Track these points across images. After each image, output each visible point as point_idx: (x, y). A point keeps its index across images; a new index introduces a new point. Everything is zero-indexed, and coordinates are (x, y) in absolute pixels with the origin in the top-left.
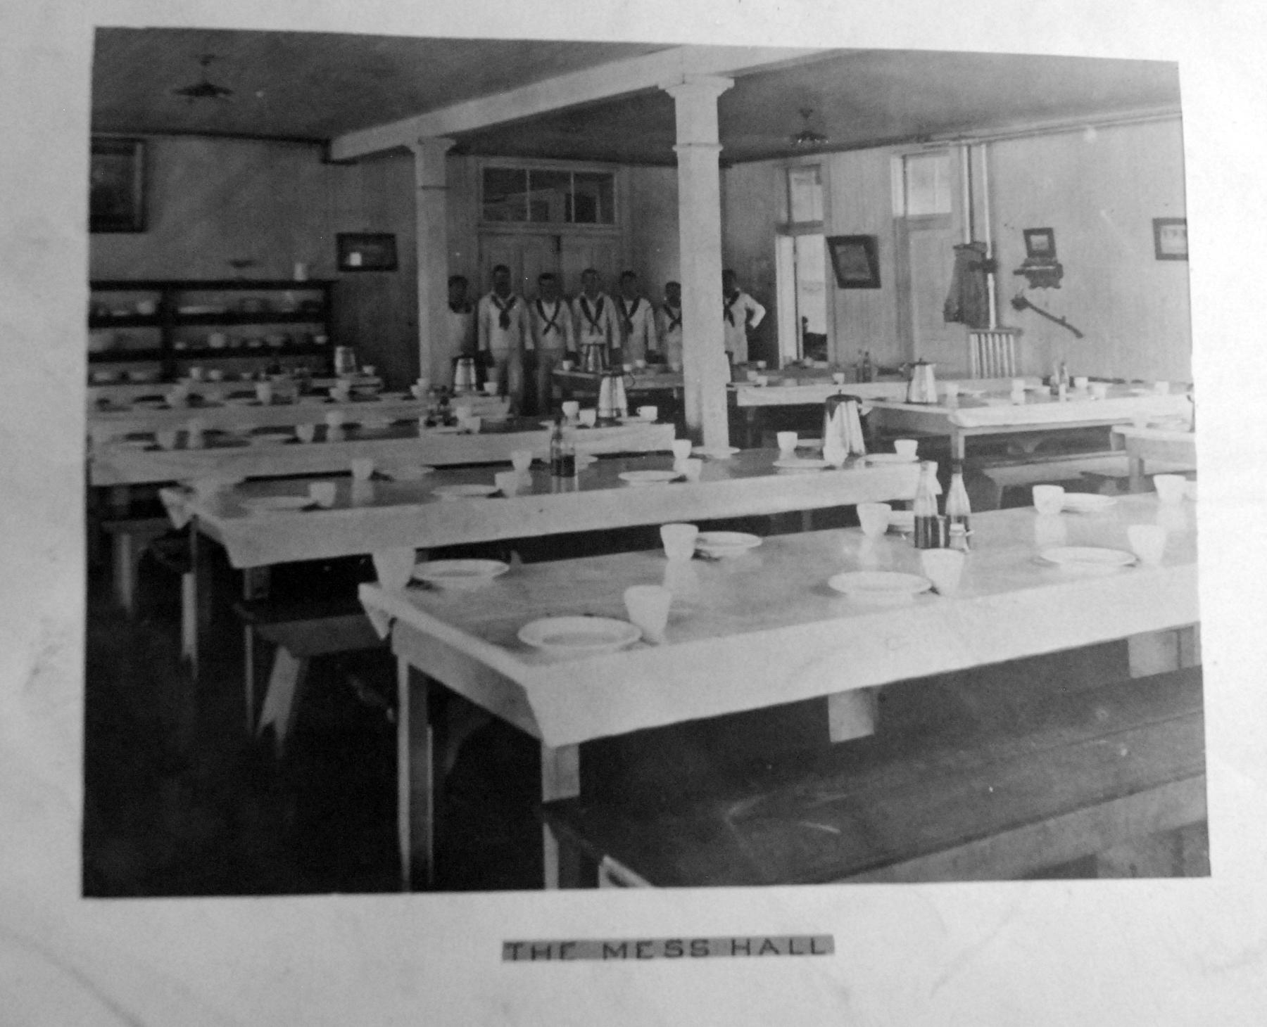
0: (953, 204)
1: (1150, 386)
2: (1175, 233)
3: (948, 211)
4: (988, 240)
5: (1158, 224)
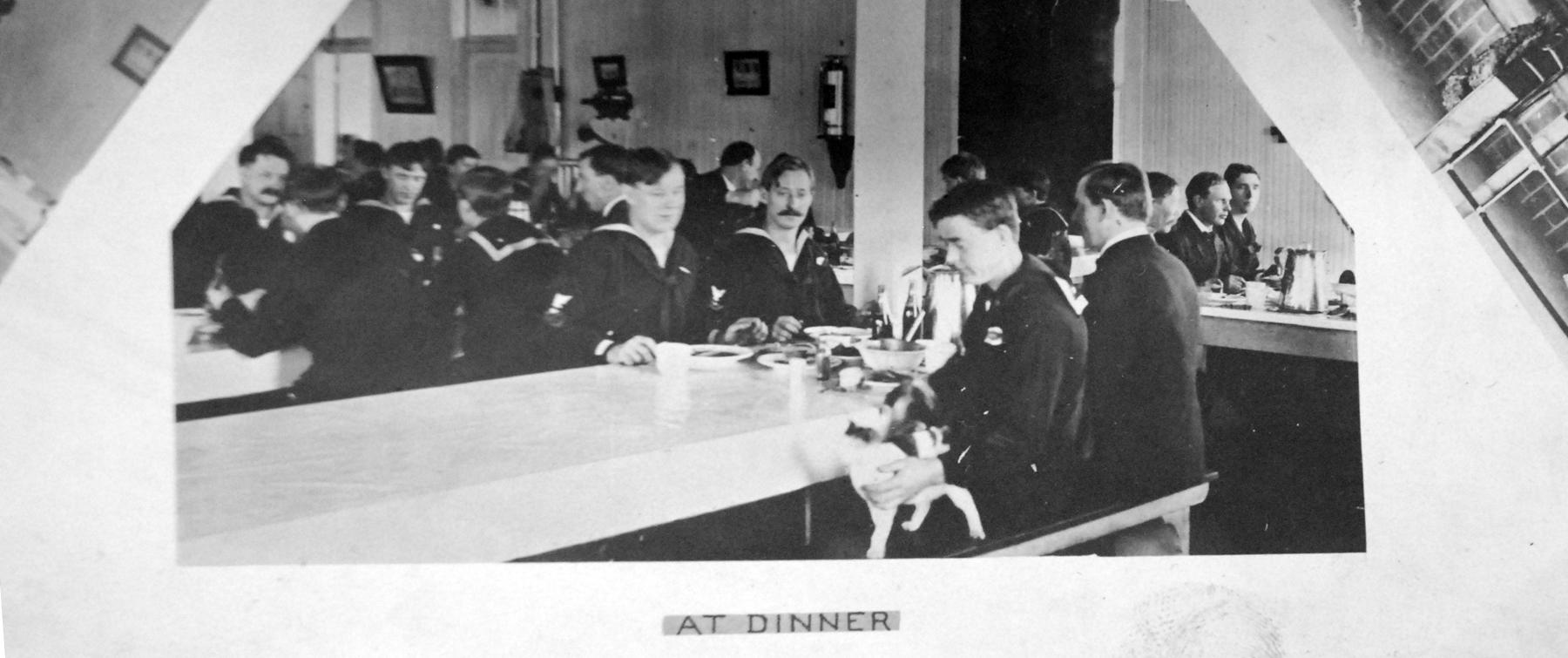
0: (519, 27)
1: (14, 173)
2: (149, 53)
3: (513, 31)
4: (556, 67)
5: (139, 33)
